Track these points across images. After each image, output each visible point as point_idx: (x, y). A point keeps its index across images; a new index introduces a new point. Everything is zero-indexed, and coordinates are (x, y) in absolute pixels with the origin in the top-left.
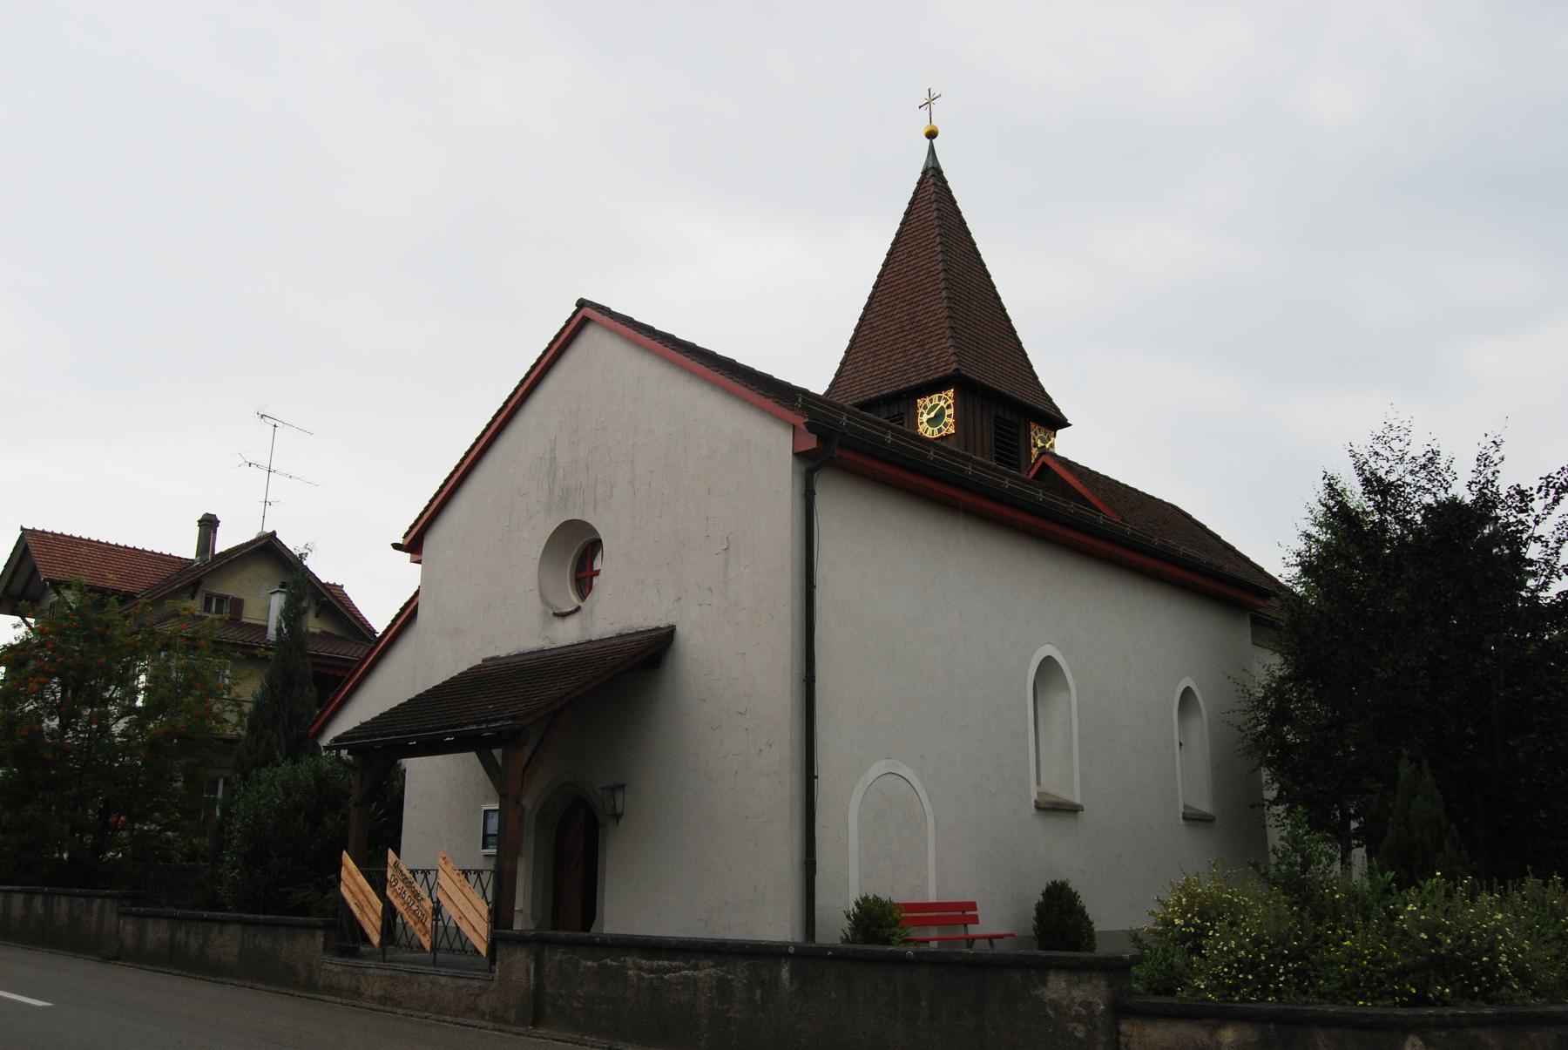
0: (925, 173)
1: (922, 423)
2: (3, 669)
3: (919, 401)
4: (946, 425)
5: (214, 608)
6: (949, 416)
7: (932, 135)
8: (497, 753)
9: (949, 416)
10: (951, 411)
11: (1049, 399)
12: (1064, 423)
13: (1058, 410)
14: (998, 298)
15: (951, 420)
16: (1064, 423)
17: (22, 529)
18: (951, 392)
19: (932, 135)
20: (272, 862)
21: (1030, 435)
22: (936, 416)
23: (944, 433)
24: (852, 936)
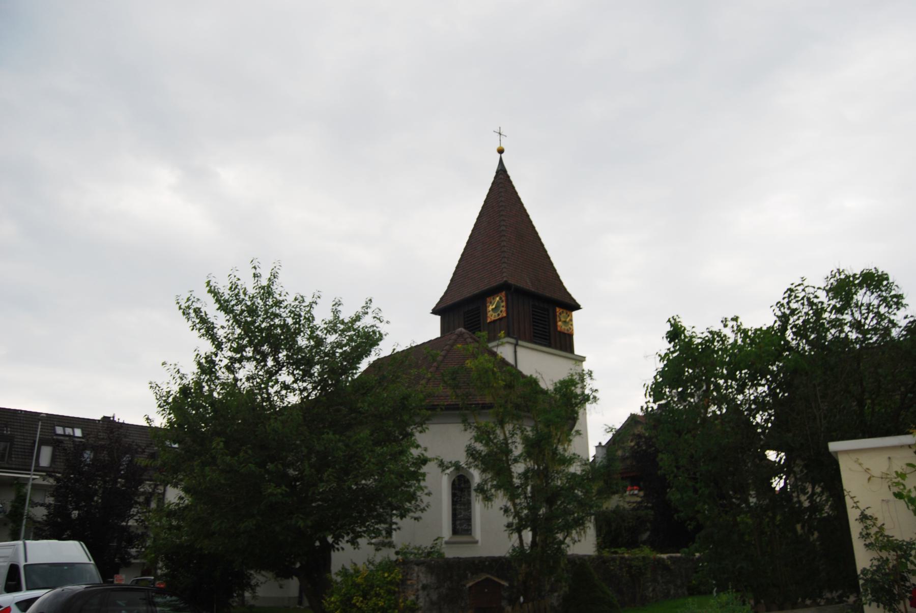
0: (497, 172)
1: (489, 311)
2: (123, 612)
3: (488, 299)
4: (501, 312)
5: (112, 580)
6: (503, 307)
7: (501, 151)
8: (510, 463)
9: (503, 307)
10: (504, 304)
11: (569, 295)
12: (577, 307)
13: (574, 301)
14: (542, 245)
15: (504, 309)
16: (577, 307)
17: (675, 333)
18: (504, 292)
19: (501, 151)
20: (382, 594)
21: (556, 315)
22: (496, 307)
23: (500, 316)
24: (557, 542)
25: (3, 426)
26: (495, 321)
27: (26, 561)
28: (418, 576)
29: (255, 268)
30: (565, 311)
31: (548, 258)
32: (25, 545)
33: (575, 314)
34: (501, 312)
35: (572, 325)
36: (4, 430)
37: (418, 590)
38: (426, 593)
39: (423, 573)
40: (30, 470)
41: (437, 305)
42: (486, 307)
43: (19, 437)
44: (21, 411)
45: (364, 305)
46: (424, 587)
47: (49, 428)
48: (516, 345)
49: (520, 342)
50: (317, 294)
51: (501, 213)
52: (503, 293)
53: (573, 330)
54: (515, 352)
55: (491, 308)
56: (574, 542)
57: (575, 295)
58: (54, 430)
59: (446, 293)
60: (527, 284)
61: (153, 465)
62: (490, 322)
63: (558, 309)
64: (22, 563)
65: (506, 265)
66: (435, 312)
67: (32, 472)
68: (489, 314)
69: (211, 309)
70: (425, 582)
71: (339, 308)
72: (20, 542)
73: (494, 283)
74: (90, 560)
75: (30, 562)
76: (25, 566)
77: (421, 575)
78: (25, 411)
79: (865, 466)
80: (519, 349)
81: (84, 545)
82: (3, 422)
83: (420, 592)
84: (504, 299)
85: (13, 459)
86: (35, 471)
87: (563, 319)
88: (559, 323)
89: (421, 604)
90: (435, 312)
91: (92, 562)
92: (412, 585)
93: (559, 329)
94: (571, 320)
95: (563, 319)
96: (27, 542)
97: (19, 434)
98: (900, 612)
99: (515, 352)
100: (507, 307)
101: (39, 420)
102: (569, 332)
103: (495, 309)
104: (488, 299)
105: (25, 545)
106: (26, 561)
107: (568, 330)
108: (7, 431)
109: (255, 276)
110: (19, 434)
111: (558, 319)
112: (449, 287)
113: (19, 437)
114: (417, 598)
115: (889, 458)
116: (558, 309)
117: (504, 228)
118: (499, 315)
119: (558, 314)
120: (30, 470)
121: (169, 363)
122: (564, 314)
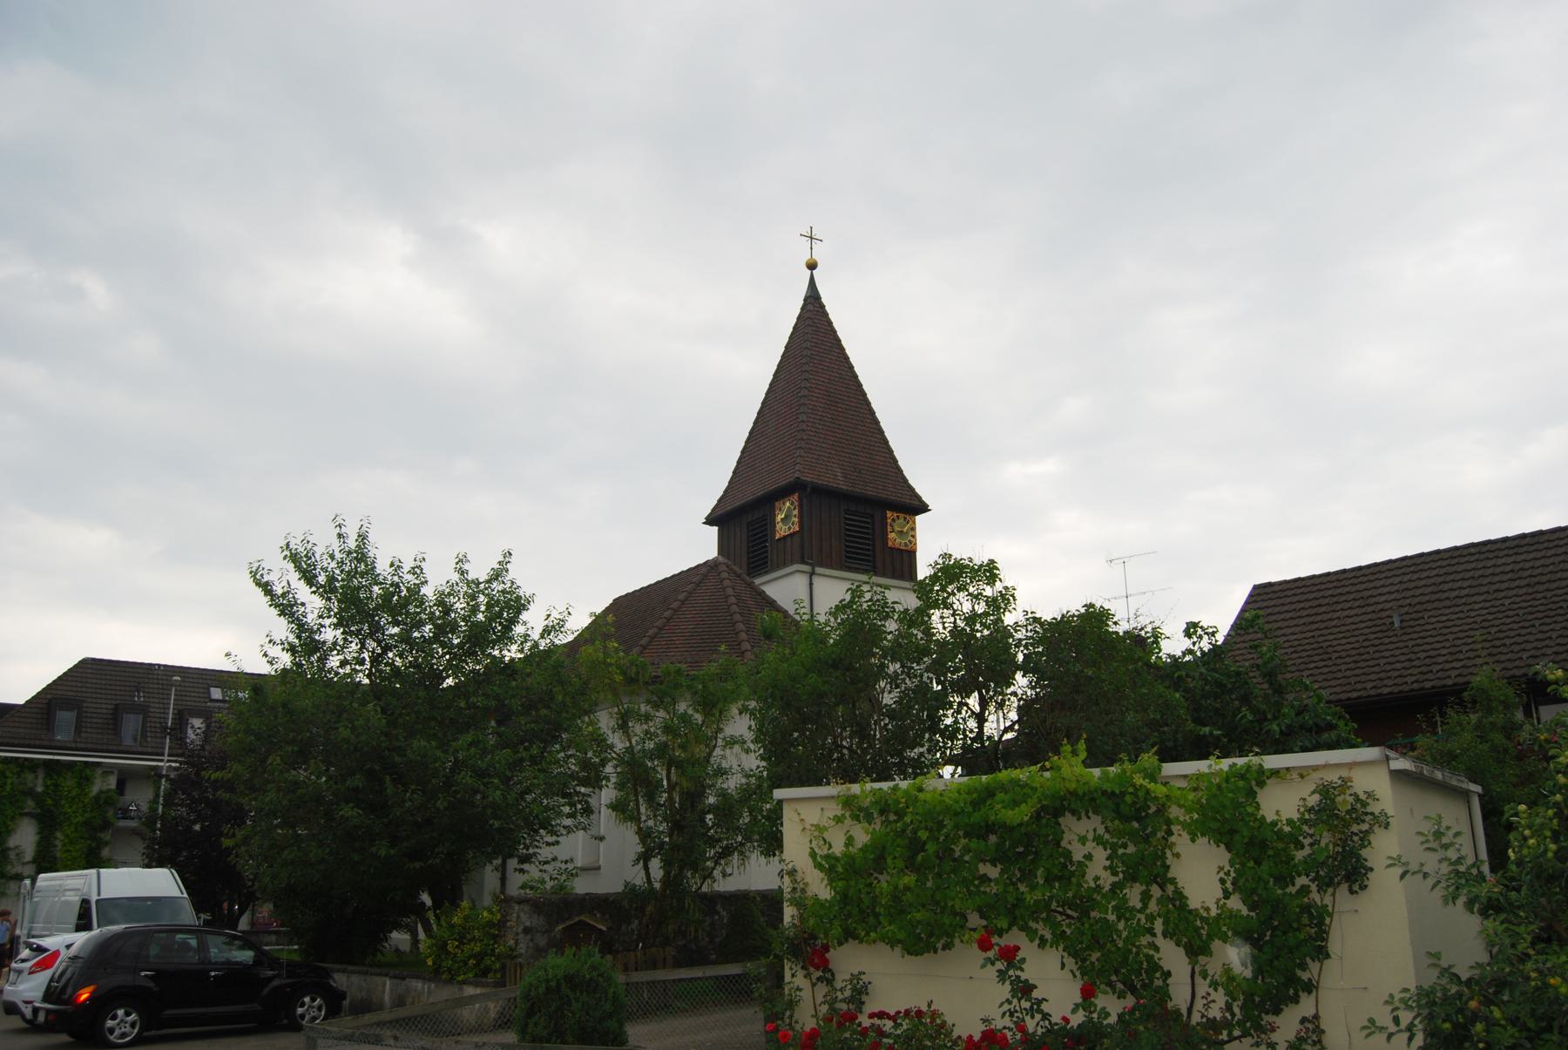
3: (777, 504)
4: (793, 524)
7: (812, 266)
10: (796, 512)
11: (912, 489)
15: (796, 520)
19: (812, 266)
22: (786, 516)
25: (133, 689)
26: (785, 537)
27: (99, 895)
28: (518, 917)
29: (340, 526)
30: (901, 515)
31: (881, 432)
32: (99, 874)
33: (920, 519)
34: (793, 524)
35: (914, 536)
36: (134, 696)
37: (517, 934)
38: (529, 937)
39: (525, 913)
40: (163, 755)
41: (713, 510)
42: (774, 516)
43: (157, 706)
44: (159, 665)
45: (501, 559)
46: (527, 931)
47: (201, 690)
48: (812, 574)
49: (818, 570)
50: (420, 557)
51: (804, 368)
52: (796, 496)
53: (915, 544)
54: (811, 584)
55: (780, 517)
56: (724, 875)
57: (921, 489)
58: (209, 693)
59: (726, 491)
60: (836, 478)
61: (212, 778)
62: (779, 539)
63: (889, 514)
64: (94, 898)
65: (802, 452)
66: (710, 521)
67: (166, 758)
68: (779, 526)
69: (285, 577)
70: (528, 924)
71: (466, 567)
72: (94, 871)
73: (783, 482)
74: (182, 893)
75: (103, 896)
76: (97, 901)
77: (522, 915)
78: (165, 666)
79: (802, 817)
80: (816, 580)
81: (176, 875)
82: (133, 684)
83: (521, 936)
84: (796, 504)
85: (149, 739)
86: (169, 755)
87: (897, 529)
88: (892, 536)
89: (522, 951)
90: (710, 521)
91: (186, 895)
92: (511, 927)
93: (890, 544)
94: (913, 529)
95: (897, 529)
96: (101, 870)
97: (157, 701)
98: (1567, 967)
99: (811, 584)
100: (801, 517)
101: (172, 686)
102: (909, 548)
103: (786, 519)
104: (777, 504)
105: (99, 874)
106: (99, 895)
107: (906, 545)
108: (139, 697)
109: (340, 536)
110: (157, 701)
111: (889, 529)
112: (730, 482)
113: (157, 706)
114: (517, 943)
115: (822, 809)
116: (889, 514)
117: (806, 392)
118: (790, 528)
119: (889, 521)
120: (163, 755)
121: (233, 654)
122: (902, 520)
